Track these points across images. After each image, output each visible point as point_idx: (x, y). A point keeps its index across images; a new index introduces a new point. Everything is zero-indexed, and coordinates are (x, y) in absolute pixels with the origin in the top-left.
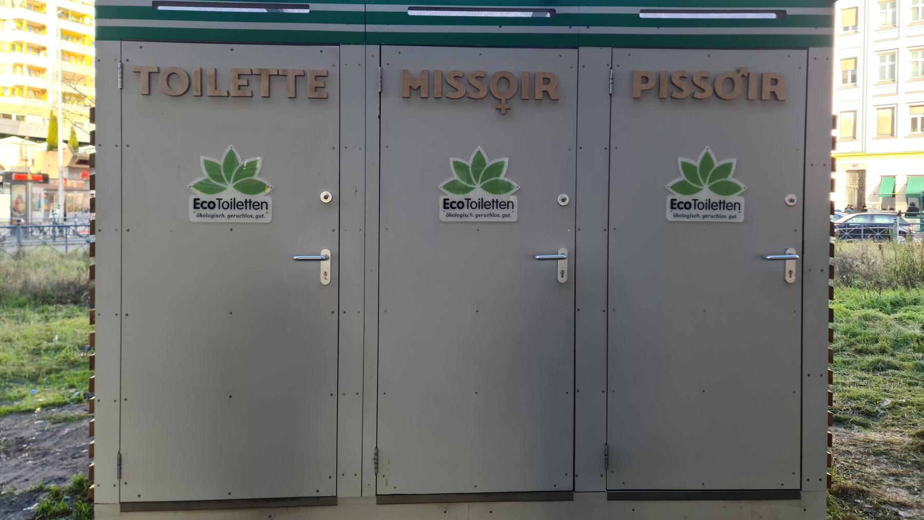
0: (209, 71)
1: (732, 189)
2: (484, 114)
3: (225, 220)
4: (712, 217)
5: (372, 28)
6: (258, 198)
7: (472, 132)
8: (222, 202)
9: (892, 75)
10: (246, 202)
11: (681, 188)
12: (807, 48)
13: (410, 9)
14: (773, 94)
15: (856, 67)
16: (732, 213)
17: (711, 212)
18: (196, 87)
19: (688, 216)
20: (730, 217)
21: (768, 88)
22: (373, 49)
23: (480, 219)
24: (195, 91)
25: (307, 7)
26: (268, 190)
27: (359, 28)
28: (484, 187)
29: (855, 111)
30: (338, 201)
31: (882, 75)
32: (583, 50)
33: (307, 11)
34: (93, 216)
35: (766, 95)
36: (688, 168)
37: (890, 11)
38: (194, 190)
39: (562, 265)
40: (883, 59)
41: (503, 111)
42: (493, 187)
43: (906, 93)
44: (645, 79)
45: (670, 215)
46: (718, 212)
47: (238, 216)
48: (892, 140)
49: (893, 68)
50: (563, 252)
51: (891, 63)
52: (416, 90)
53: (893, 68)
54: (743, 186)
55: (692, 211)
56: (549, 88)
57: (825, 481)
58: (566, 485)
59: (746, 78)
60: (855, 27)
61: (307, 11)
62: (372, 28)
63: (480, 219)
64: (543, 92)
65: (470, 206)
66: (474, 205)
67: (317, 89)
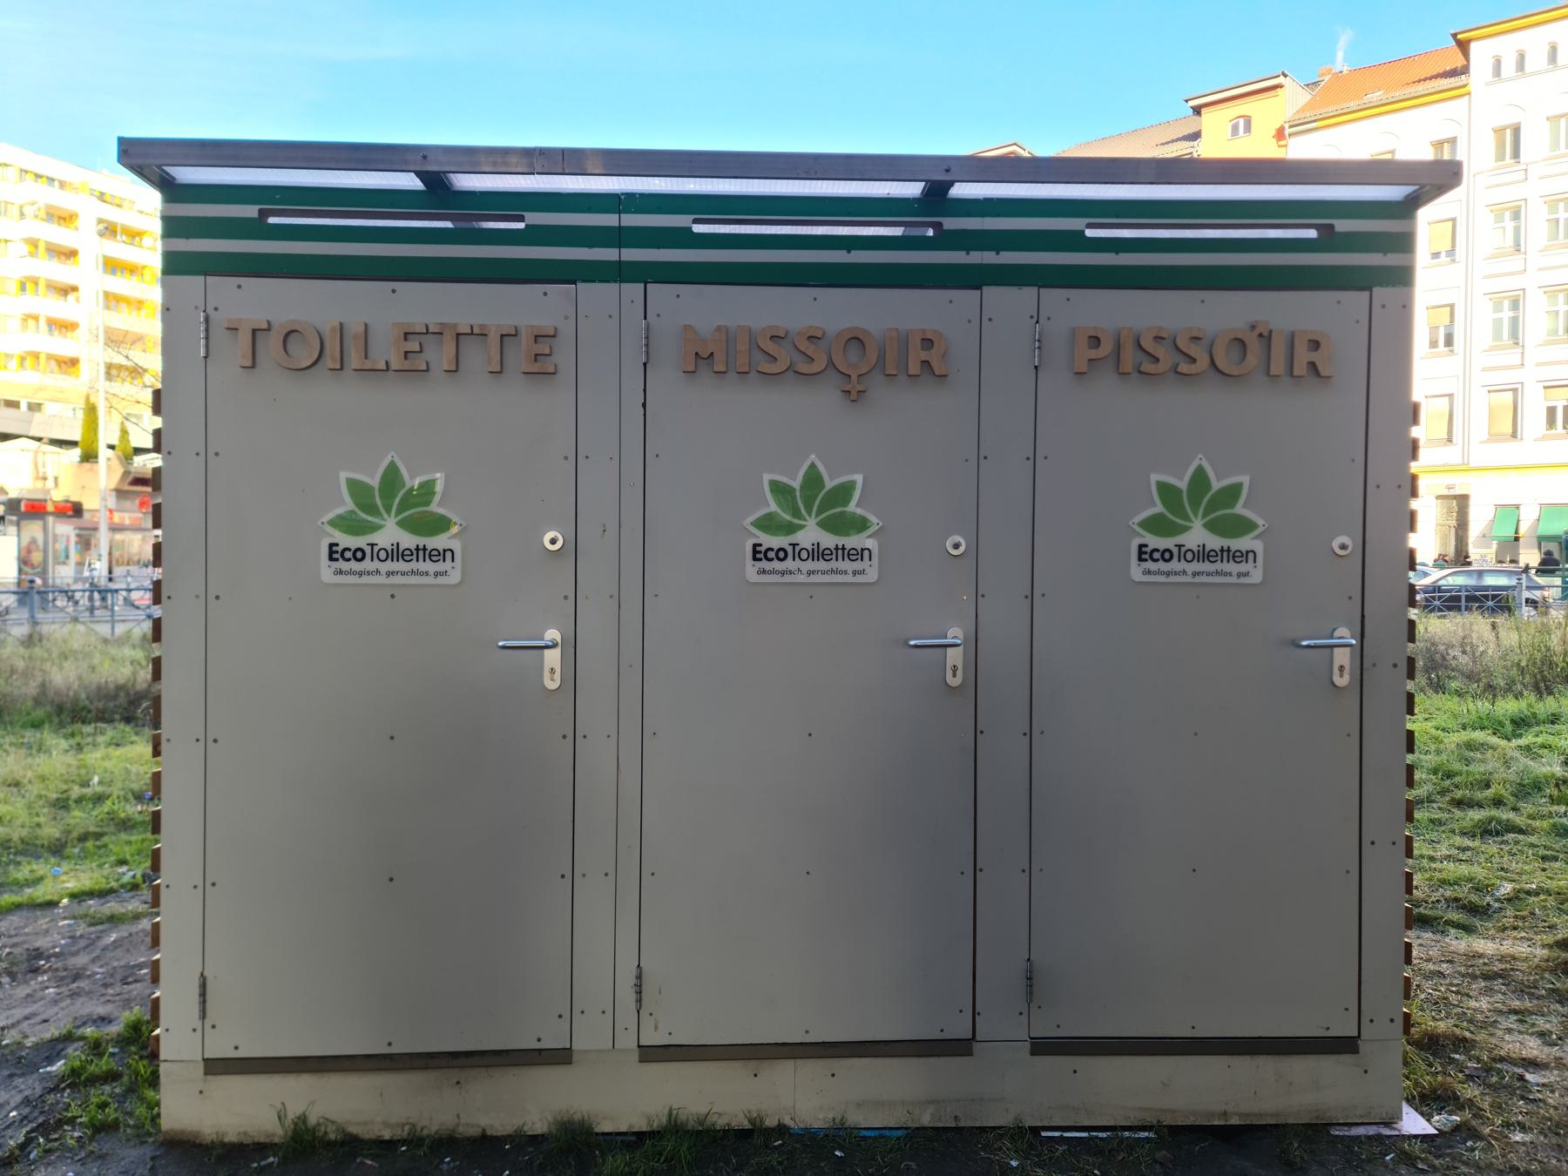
0: (354, 327)
1: (1243, 526)
2: (823, 401)
3: (381, 580)
4: (1208, 574)
5: (631, 254)
6: (438, 542)
7: (799, 430)
8: (376, 549)
9: (1514, 334)
10: (417, 549)
11: (347, 524)
12: (1370, 289)
13: (696, 221)
14: (1312, 365)
15: (1452, 321)
16: (1243, 567)
17: (1206, 566)
18: (334, 354)
19: (1168, 574)
20: (1239, 575)
21: (1303, 356)
22: (634, 290)
23: (1204, 579)
24: (330, 361)
25: (521, 219)
26: (455, 530)
27: (609, 254)
28: (824, 525)
29: (1451, 396)
30: (574, 548)
31: (1497, 335)
32: (580, 285)
33: (521, 225)
34: (157, 573)
35: (1300, 368)
36: (1166, 491)
37: (1509, 225)
38: (329, 529)
39: (954, 657)
40: (1498, 307)
41: (854, 396)
42: (836, 525)
43: (1538, 365)
44: (1095, 341)
45: (1136, 571)
46: (1218, 566)
47: (1208, 574)
48: (1514, 444)
49: (1514, 322)
50: (955, 634)
51: (1511, 314)
52: (704, 360)
53: (1514, 322)
54: (1260, 522)
55: (1175, 565)
56: (933, 356)
57: (1399, 1021)
58: (958, 1028)
59: (1266, 338)
60: (1451, 253)
61: (521, 225)
62: (631, 254)
63: (1204, 579)
64: (921, 362)
65: (797, 555)
66: (804, 555)
67: (537, 357)
